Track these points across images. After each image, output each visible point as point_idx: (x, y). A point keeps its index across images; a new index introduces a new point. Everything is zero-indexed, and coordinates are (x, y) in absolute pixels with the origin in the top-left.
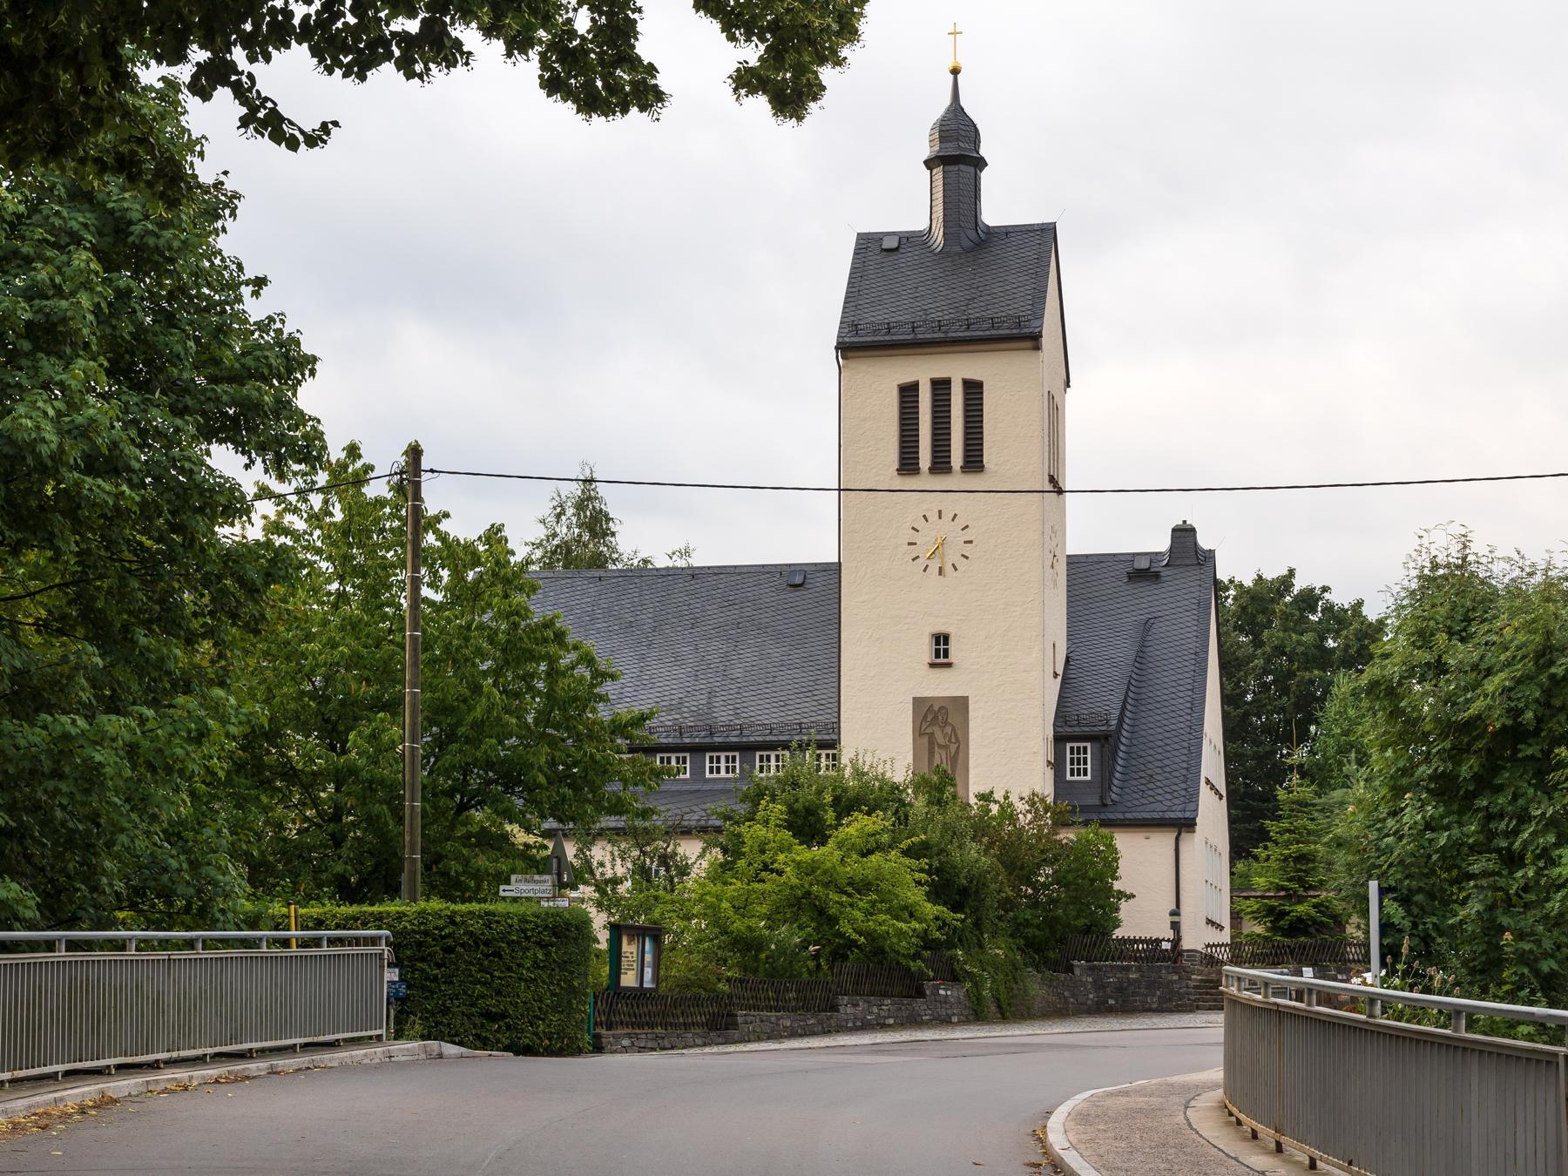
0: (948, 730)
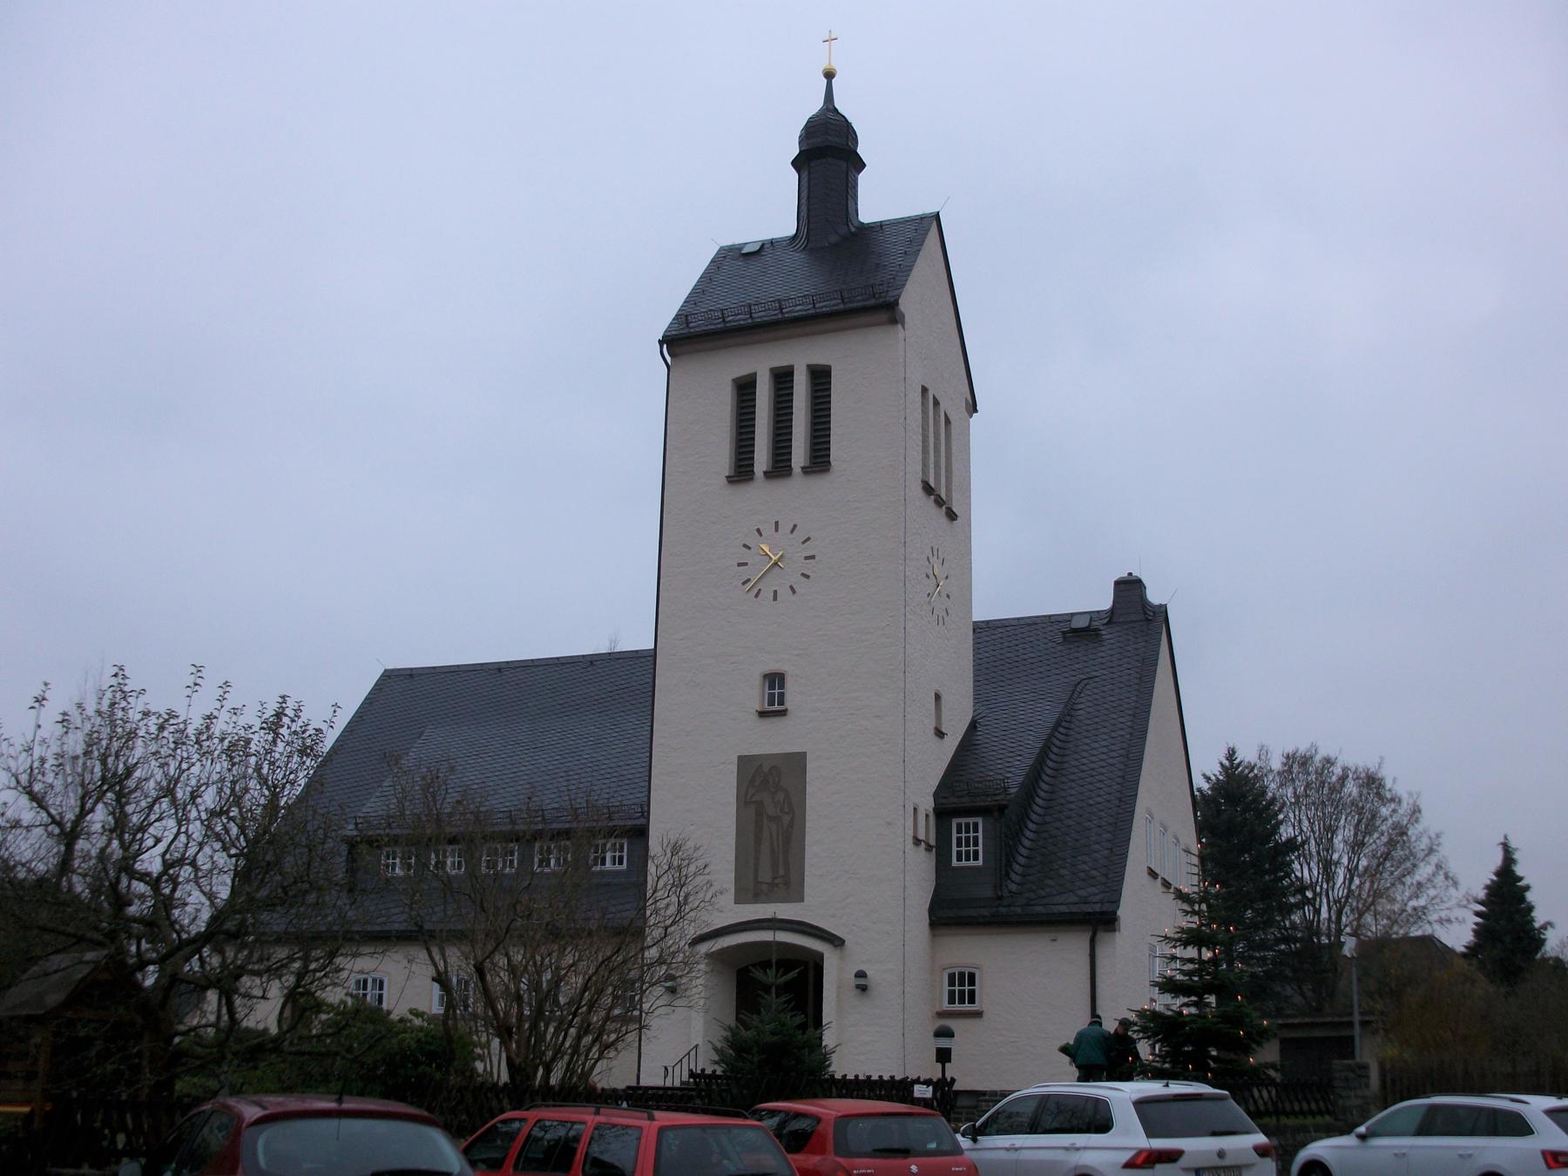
0: (780, 796)
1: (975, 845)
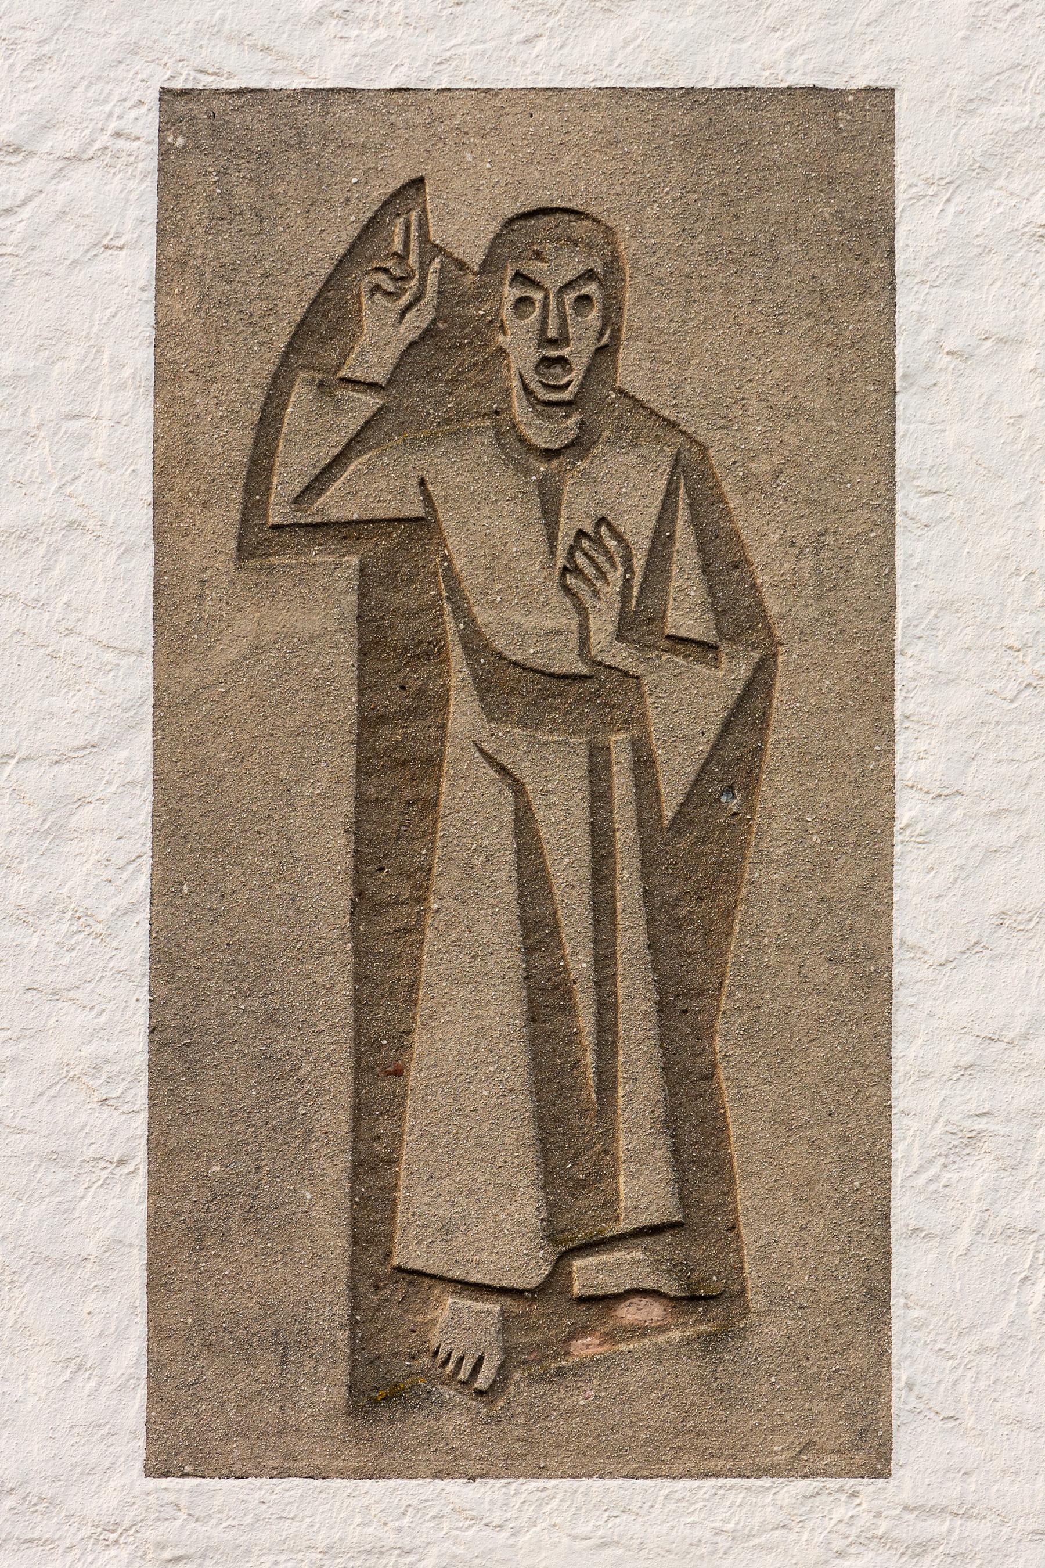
0: (626, 488)
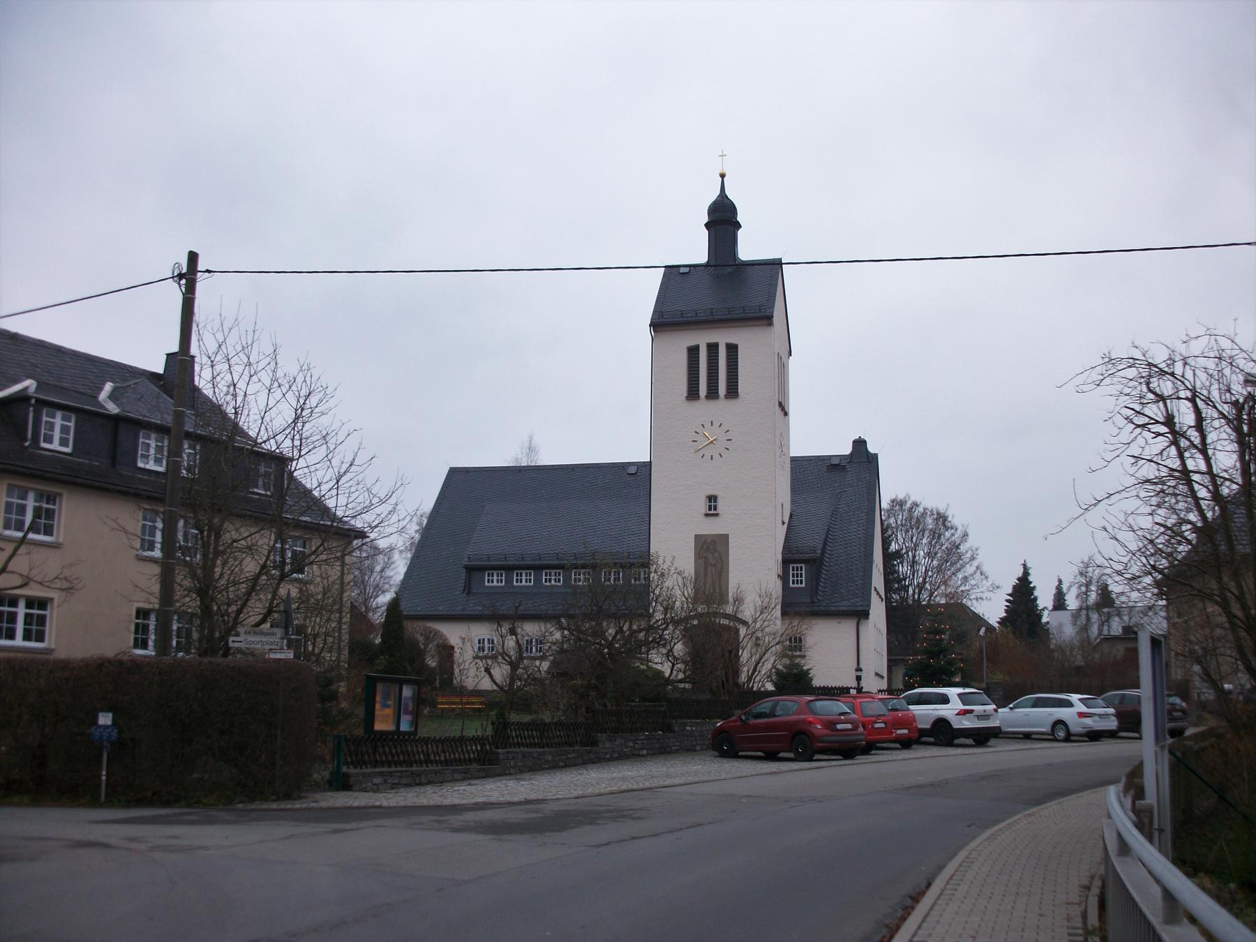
0: (716, 555)
1: (800, 579)
